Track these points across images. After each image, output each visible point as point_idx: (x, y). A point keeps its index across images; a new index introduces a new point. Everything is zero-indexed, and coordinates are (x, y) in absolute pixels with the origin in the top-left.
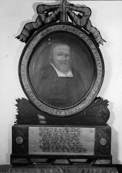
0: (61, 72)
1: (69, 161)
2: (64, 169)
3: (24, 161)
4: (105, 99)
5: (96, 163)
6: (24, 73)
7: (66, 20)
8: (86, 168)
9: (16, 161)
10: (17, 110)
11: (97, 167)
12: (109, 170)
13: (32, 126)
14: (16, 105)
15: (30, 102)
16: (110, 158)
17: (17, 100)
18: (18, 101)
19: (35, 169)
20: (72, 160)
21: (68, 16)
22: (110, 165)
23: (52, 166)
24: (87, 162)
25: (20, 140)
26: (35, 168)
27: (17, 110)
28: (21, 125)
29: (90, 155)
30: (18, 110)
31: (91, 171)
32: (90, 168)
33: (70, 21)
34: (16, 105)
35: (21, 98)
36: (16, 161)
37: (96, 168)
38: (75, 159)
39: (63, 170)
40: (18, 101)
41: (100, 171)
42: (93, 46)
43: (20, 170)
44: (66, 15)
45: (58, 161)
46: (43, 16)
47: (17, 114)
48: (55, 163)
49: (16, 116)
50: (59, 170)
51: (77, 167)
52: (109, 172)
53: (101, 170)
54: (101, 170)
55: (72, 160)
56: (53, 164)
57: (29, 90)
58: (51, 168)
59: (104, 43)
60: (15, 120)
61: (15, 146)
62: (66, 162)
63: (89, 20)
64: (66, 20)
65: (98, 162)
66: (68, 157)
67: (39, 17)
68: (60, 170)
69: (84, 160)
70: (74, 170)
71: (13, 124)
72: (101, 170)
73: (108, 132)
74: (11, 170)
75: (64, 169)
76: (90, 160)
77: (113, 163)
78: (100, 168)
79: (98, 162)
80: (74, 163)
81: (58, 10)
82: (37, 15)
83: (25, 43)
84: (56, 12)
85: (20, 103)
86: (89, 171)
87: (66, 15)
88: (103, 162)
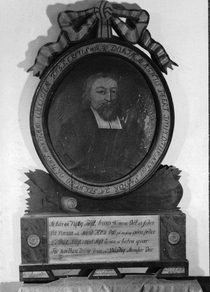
0: (105, 119)
1: (118, 272)
2: (111, 286)
3: (44, 275)
4: (177, 165)
5: (164, 272)
6: (38, 129)
7: (108, 34)
8: (147, 283)
9: (27, 275)
10: (28, 190)
11: (165, 280)
12: (185, 286)
13: (57, 215)
14: (25, 183)
15: (51, 177)
16: (186, 265)
17: (27, 174)
18: (30, 175)
19: (62, 287)
20: (123, 270)
21: (47, 172)
22: (185, 277)
23: (91, 281)
24: (148, 273)
25: (34, 241)
26: (63, 285)
27: (28, 190)
28: (146, 51)
29: (117, 261)
30: (29, 191)
31: (155, 288)
32: (155, 284)
33: (114, 33)
34: (25, 183)
35: (34, 170)
36: (27, 275)
37: (164, 282)
38: (126, 268)
39: (109, 287)
40: (30, 175)
41: (170, 287)
42: (154, 80)
43: (38, 289)
44: (108, 27)
45: (99, 273)
46: (70, 30)
47: (29, 197)
48: (94, 275)
49: (27, 200)
50: (102, 288)
51: (132, 282)
52: (186, 290)
53: (172, 287)
54: (172, 286)
55: (123, 270)
56: (92, 278)
57: (47, 154)
58: (90, 285)
59: (173, 66)
60: (25, 207)
61: (26, 253)
62: (113, 273)
63: (147, 31)
64: (108, 34)
65: (166, 271)
66: (114, 266)
67: (64, 33)
68: (105, 287)
69: (144, 270)
70: (127, 287)
71: (22, 214)
72: (172, 287)
73: (181, 219)
74: (21, 290)
75: (111, 286)
76: (154, 268)
77: (190, 274)
78: (171, 283)
79: (166, 271)
80: (126, 276)
81: (94, 17)
82: (59, 31)
83: (40, 78)
84: (90, 22)
85: (33, 178)
86: (158, 289)
87: (108, 27)
88: (179, 271)
